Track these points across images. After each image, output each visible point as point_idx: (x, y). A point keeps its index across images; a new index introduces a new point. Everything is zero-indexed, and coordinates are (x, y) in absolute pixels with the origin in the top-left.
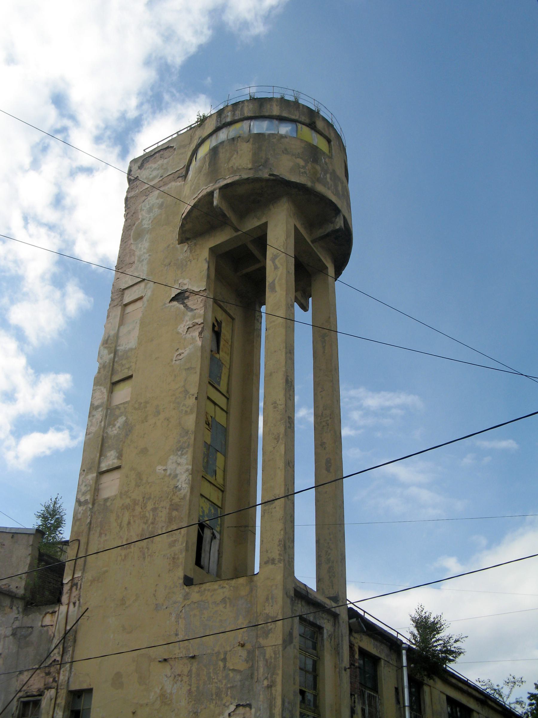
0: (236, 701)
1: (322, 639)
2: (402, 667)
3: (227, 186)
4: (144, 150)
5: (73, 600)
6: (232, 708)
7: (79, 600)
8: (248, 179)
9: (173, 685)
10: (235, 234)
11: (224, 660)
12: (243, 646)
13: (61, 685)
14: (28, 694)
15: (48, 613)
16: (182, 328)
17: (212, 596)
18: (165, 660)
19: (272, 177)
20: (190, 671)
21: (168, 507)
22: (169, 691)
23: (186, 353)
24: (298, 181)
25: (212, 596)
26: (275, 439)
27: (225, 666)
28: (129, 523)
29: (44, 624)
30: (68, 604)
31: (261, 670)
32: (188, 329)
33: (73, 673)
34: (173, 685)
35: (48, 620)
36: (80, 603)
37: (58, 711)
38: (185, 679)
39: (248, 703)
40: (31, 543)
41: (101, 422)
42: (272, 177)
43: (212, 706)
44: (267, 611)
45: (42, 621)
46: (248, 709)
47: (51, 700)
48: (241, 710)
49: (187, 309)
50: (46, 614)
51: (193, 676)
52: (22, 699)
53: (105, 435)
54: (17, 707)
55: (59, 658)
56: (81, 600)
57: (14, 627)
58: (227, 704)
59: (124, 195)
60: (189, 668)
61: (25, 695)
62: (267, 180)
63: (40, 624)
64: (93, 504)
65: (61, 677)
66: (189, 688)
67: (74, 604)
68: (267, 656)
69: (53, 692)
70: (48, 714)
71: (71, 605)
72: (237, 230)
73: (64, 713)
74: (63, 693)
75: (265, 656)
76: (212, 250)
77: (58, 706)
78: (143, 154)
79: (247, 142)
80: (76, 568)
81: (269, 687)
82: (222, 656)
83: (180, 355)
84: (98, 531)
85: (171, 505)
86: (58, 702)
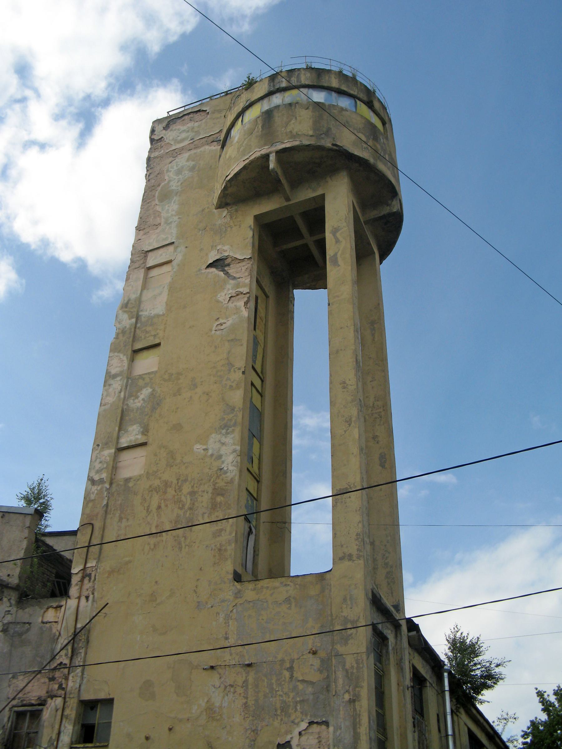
0: (309, 718)
1: (387, 652)
2: (443, 691)
3: (285, 150)
4: (168, 113)
5: (85, 593)
6: (304, 725)
7: (93, 594)
8: (308, 146)
9: (224, 697)
10: (286, 204)
11: (291, 669)
12: (314, 653)
13: (71, 693)
14: (25, 702)
15: (51, 607)
16: (223, 296)
17: (271, 595)
18: (212, 667)
19: (335, 148)
20: (246, 682)
21: (210, 490)
22: (217, 704)
23: (229, 323)
24: (361, 156)
25: (271, 595)
26: (346, 421)
27: (292, 677)
28: (159, 507)
29: (45, 620)
30: (79, 598)
31: (340, 681)
32: (230, 298)
33: (85, 680)
34: (224, 697)
35: (50, 615)
36: (94, 597)
37: (67, 725)
38: (240, 690)
39: (324, 720)
40: (28, 524)
41: (120, 392)
42: (335, 148)
43: (276, 723)
44: (344, 614)
45: (43, 617)
46: (324, 727)
47: (57, 710)
48: (315, 728)
49: (228, 277)
50: (48, 608)
51: (250, 687)
52: (16, 709)
53: (125, 407)
54: (9, 718)
55: (66, 661)
56: (96, 594)
57: (5, 622)
58: (296, 721)
59: (148, 150)
60: (244, 678)
61: (20, 704)
62: (330, 150)
63: (40, 620)
64: (111, 484)
65: (70, 684)
66: (244, 701)
67: (87, 598)
68: (348, 666)
69: (59, 701)
70: (53, 727)
71: (83, 600)
72: (288, 199)
73: (74, 727)
74: (73, 703)
75: (344, 666)
76: (256, 218)
77: (67, 718)
78: (166, 116)
79: (307, 109)
80: (89, 557)
81: (352, 701)
82: (288, 665)
83: (221, 324)
84: (117, 515)
85: (214, 489)
86: (65, 713)
